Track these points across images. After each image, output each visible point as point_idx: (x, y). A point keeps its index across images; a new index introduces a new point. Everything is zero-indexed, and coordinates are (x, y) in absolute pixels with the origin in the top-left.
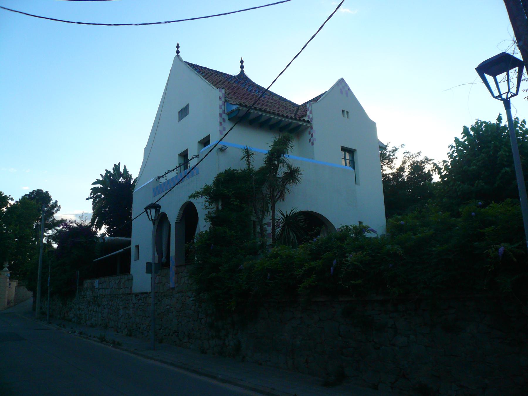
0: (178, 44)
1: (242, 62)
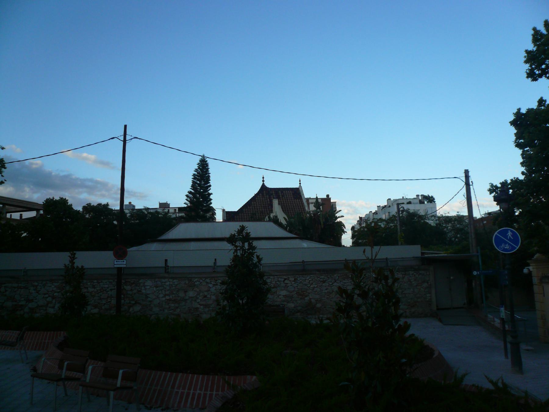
1: (263, 178)
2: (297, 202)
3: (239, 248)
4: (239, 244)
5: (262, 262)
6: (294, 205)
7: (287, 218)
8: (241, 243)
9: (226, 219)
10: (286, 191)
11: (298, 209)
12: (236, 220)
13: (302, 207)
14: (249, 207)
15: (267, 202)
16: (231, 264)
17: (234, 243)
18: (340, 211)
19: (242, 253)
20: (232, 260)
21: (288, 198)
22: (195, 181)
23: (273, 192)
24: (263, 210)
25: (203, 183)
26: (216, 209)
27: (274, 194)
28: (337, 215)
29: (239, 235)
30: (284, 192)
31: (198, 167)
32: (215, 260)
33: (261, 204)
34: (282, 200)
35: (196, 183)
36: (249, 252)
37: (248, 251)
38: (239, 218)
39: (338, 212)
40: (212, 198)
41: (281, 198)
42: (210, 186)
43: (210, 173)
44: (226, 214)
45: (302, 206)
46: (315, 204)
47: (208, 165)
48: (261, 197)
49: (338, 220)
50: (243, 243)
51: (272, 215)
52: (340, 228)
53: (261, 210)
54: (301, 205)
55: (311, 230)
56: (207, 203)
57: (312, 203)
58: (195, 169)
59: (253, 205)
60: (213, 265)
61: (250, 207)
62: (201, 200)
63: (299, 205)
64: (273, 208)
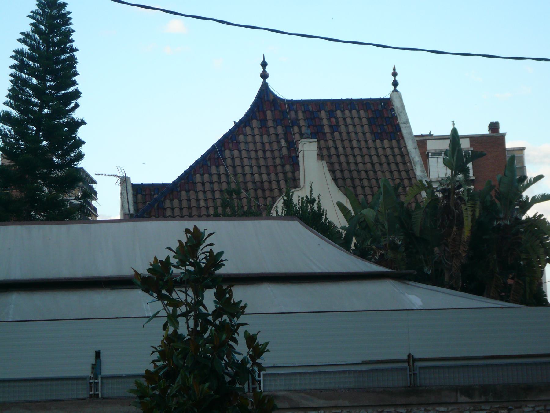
0: (394, 69)
2: (384, 149)
3: (183, 309)
4: (183, 296)
5: (265, 360)
6: (375, 159)
7: (349, 206)
8: (190, 292)
9: (132, 212)
10: (347, 112)
11: (388, 174)
12: (169, 213)
13: (401, 167)
14: (214, 170)
15: (280, 150)
16: (156, 366)
17: (164, 292)
18: (540, 177)
19: (196, 325)
20: (160, 352)
21: (353, 135)
22: (23, 75)
23: (301, 115)
24: (265, 177)
25: (52, 83)
26: (95, 178)
27: (302, 123)
28: (529, 193)
29: (182, 263)
30: (339, 113)
31: (32, 24)
32: (98, 354)
33: (257, 159)
34: (331, 143)
35: (25, 83)
36: (217, 322)
37: (215, 319)
38: (181, 209)
39: (530, 184)
40: (83, 139)
41: (329, 136)
42: (77, 94)
43: (76, 50)
44: (135, 195)
45: (404, 163)
46: (449, 153)
47: (70, 19)
48: (256, 131)
49: (530, 213)
50: (199, 293)
51: (297, 196)
52: (321, 209)
53: (257, 177)
54: (399, 159)
55: (436, 249)
56: (66, 153)
57: (437, 154)
58: (22, 33)
59: (229, 161)
60: (87, 372)
61: (218, 166)
62: (45, 143)
63: (391, 158)
64: (299, 170)
